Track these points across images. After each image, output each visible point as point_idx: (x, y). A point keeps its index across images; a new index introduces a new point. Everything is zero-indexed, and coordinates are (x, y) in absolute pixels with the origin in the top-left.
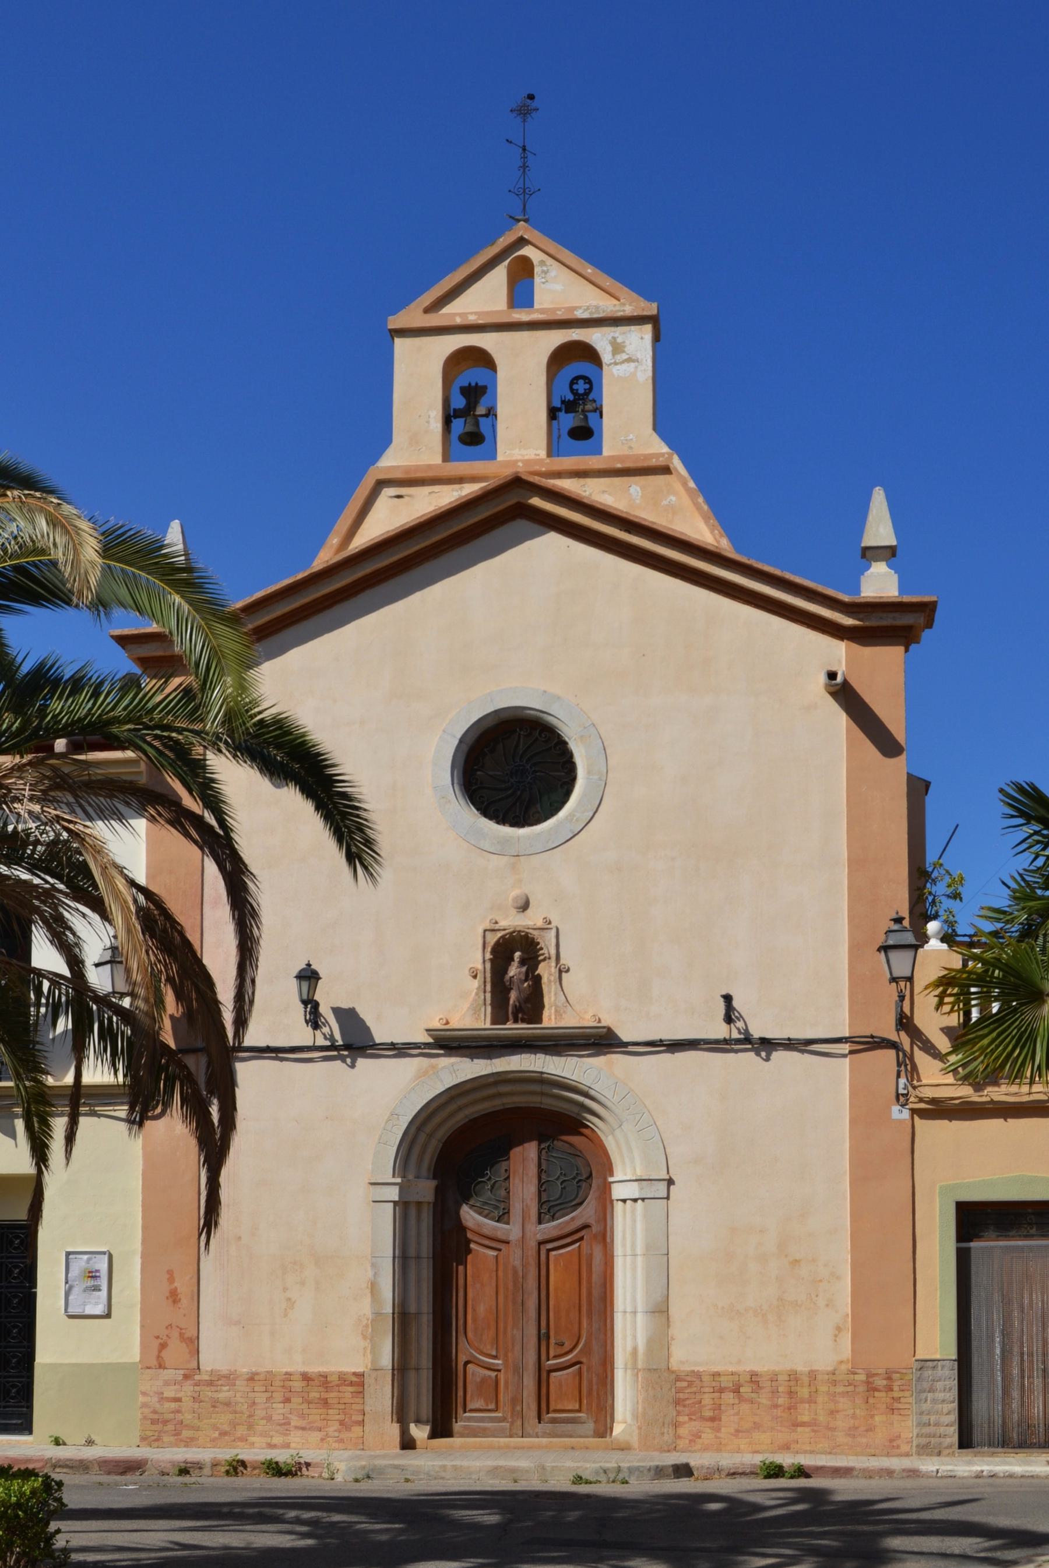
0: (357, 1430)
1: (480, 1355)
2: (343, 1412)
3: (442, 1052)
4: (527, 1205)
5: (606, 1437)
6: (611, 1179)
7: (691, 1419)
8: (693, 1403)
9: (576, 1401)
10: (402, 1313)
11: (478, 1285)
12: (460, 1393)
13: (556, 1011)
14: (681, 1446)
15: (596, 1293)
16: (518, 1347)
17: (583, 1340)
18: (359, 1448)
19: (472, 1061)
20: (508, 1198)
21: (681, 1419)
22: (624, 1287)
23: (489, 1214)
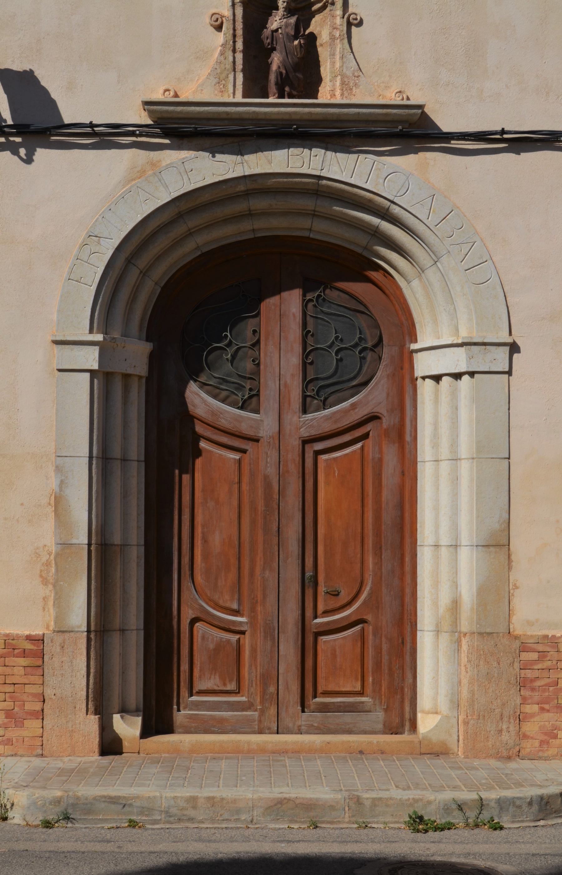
0: (33, 725)
1: (214, 609)
2: (11, 697)
3: (167, 141)
4: (286, 385)
5: (401, 733)
6: (414, 346)
7: (542, 709)
8: (546, 685)
9: (357, 679)
10: (102, 545)
11: (211, 504)
12: (185, 667)
13: (343, 83)
14: (528, 750)
15: (388, 517)
16: (272, 598)
17: (368, 588)
18: (35, 753)
19: (214, 156)
20: (258, 373)
21: (529, 709)
22: (436, 508)
23: (227, 397)
